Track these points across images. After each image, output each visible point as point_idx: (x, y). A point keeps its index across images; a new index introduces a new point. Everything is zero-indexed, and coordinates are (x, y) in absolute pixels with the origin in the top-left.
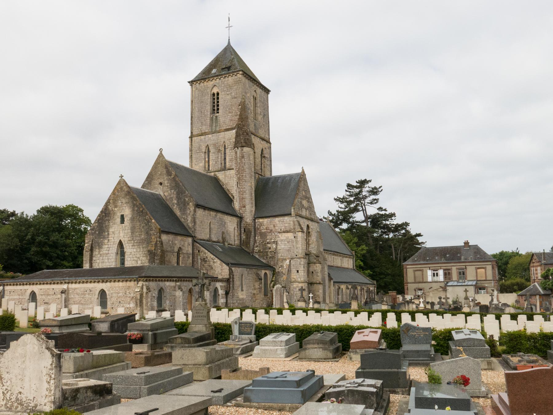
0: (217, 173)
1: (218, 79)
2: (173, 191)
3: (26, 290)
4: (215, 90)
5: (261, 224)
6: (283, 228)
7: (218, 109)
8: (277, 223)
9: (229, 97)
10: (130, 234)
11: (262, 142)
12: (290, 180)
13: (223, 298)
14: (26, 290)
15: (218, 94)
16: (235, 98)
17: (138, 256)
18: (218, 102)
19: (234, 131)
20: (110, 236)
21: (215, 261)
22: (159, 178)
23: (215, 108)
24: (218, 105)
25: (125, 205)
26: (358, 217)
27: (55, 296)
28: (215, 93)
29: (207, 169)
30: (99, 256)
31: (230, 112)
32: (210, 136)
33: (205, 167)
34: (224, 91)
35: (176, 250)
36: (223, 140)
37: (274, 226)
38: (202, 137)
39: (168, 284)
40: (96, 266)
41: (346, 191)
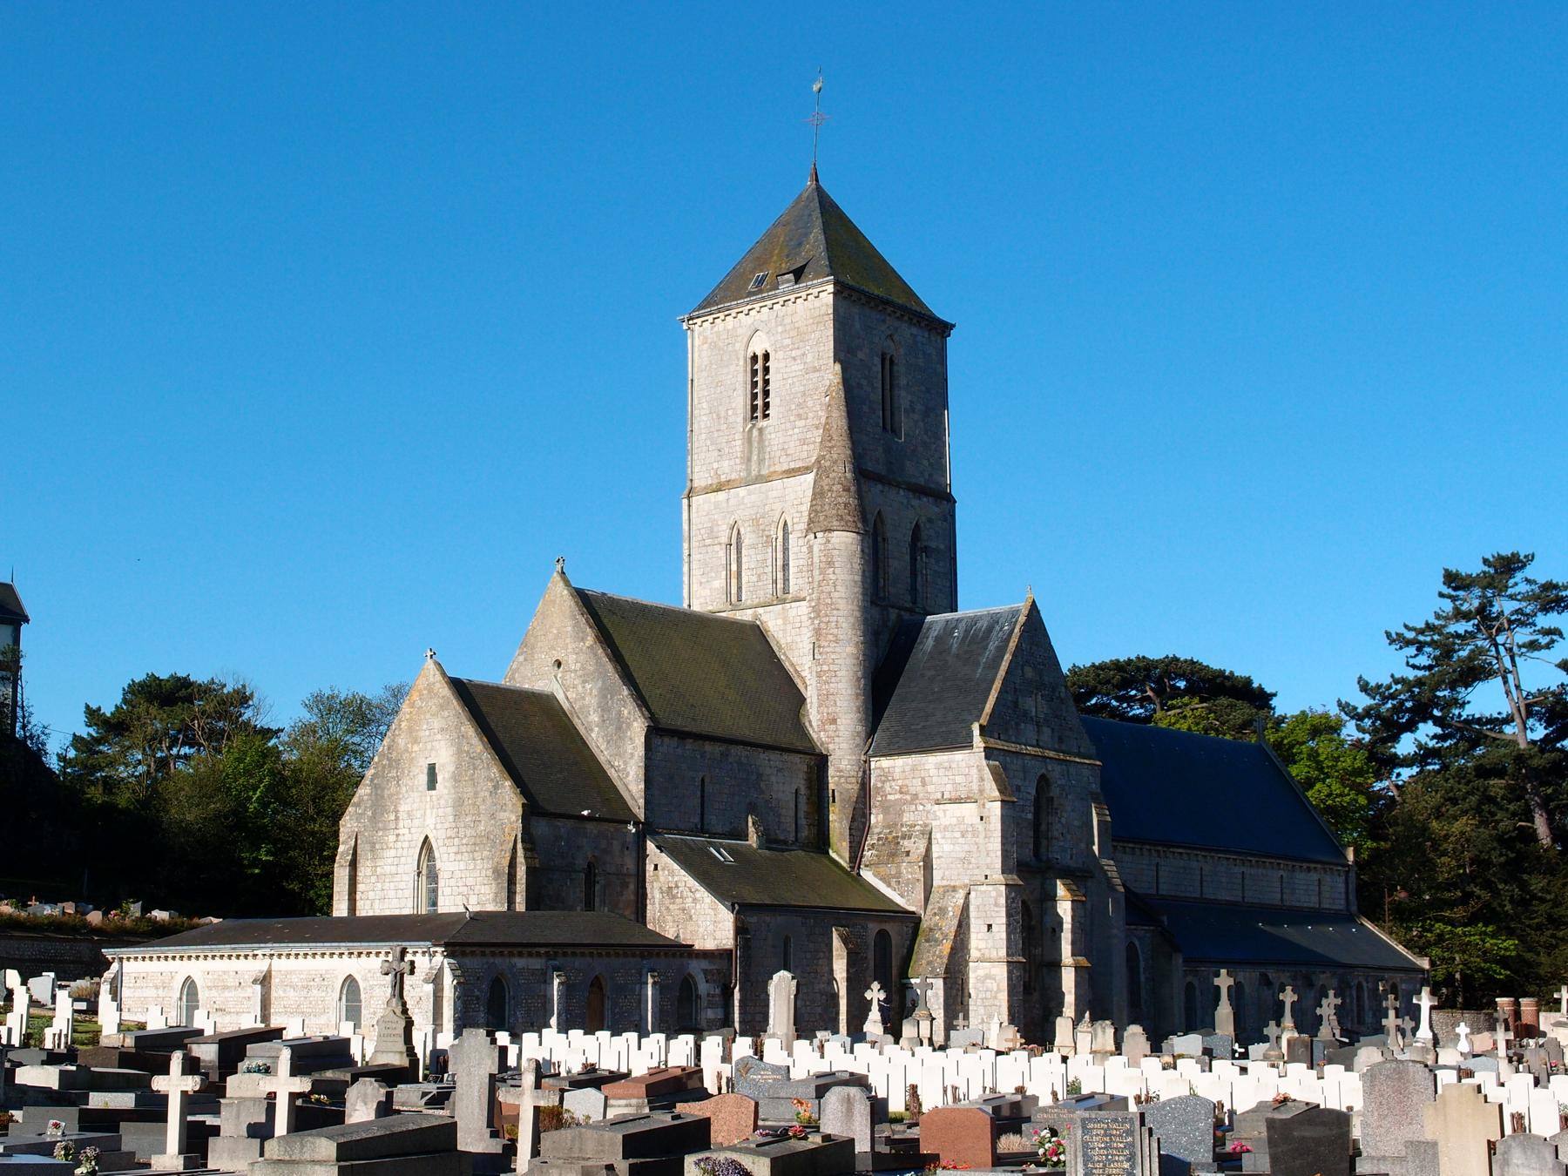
0: (760, 610)
1: (765, 310)
2: (588, 686)
3: (172, 975)
4: (758, 348)
5: (887, 776)
6: (949, 787)
7: (767, 406)
8: (932, 772)
9: (797, 367)
10: (451, 818)
11: (915, 502)
12: (990, 629)
13: (711, 1005)
14: (172, 975)
15: (766, 357)
16: (816, 370)
17: (470, 881)
18: (766, 382)
19: (810, 477)
21: (698, 895)
22: (553, 648)
23: (759, 406)
24: (766, 393)
25: (439, 737)
26: (1485, 700)
27: (241, 993)
28: (760, 354)
29: (734, 599)
30: (373, 879)
31: (799, 416)
32: (742, 491)
33: (728, 593)
34: (783, 347)
35: (581, 863)
36: (778, 507)
37: (924, 784)
38: (721, 496)
39: (520, 963)
40: (364, 910)
41: (1441, 595)
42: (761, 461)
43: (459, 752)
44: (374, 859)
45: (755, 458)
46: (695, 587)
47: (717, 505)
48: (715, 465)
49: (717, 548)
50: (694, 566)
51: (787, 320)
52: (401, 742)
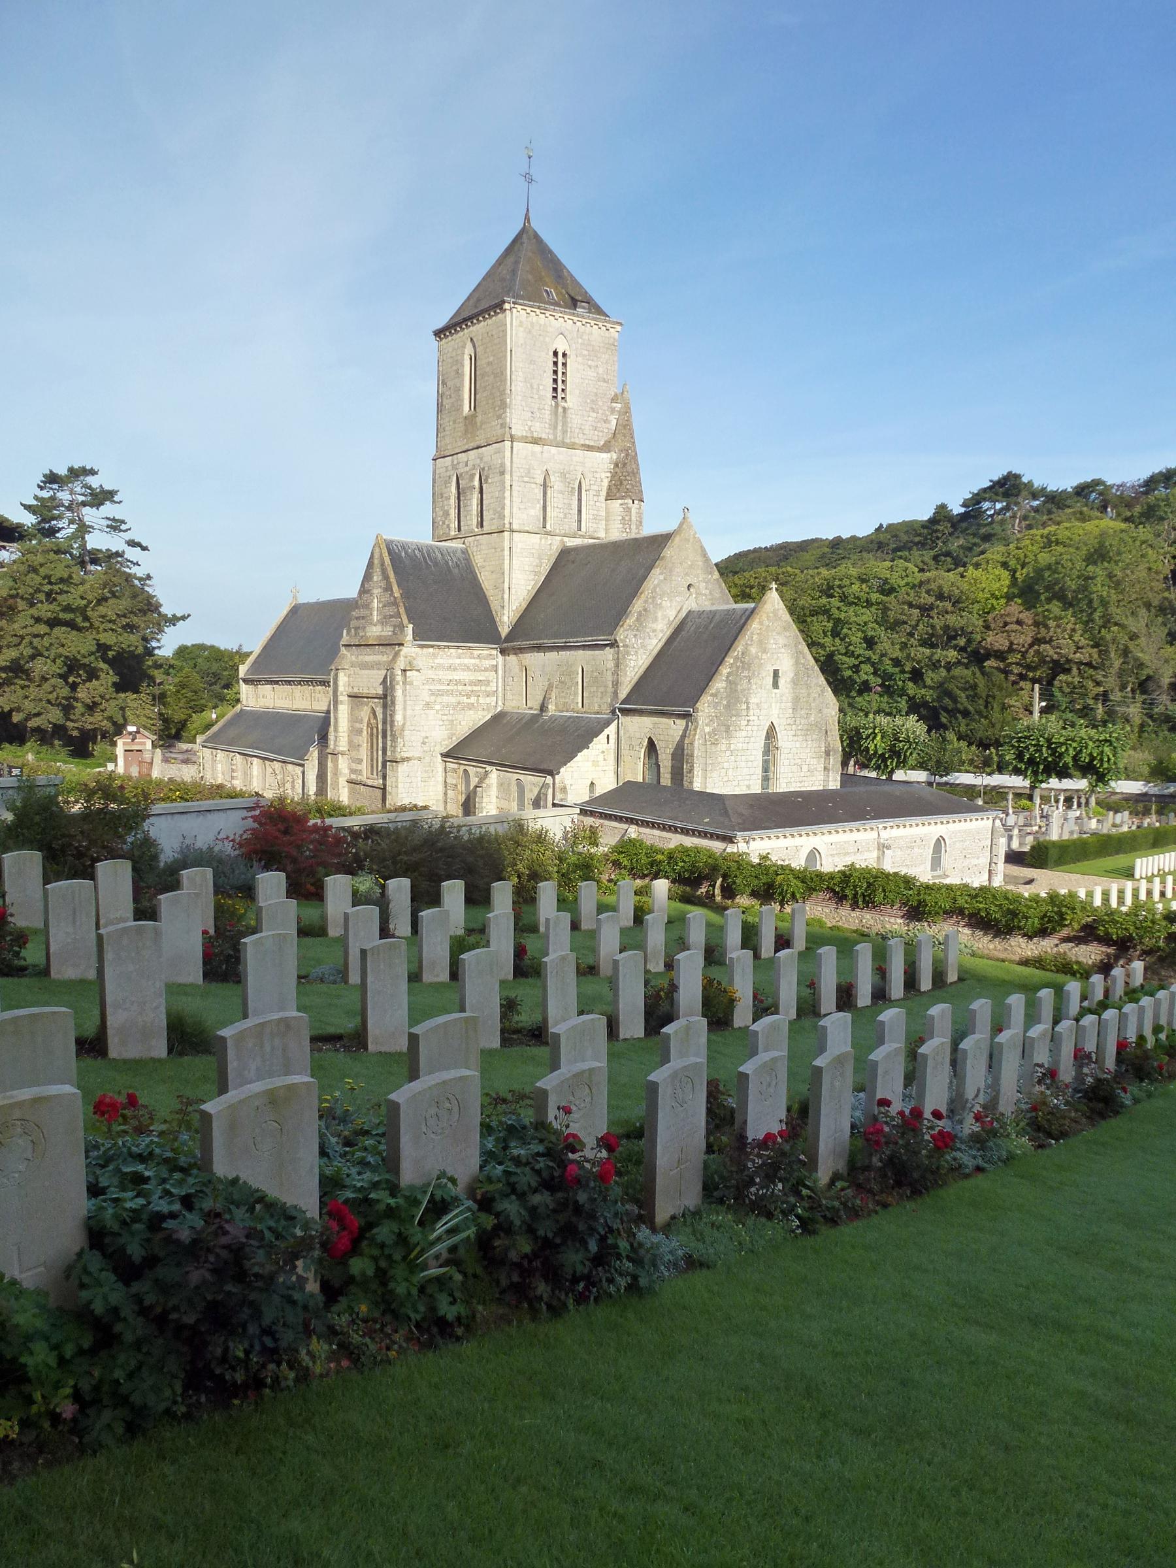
16: (604, 381)
17: (803, 756)
20: (751, 712)
22: (687, 574)
30: (728, 753)
31: (593, 410)
32: (553, 450)
36: (580, 469)
38: (537, 448)
42: (564, 432)
43: (797, 663)
44: (729, 737)
45: (560, 428)
46: (515, 510)
47: (533, 453)
48: (529, 423)
49: (533, 486)
50: (515, 494)
51: (586, 337)
52: (753, 650)
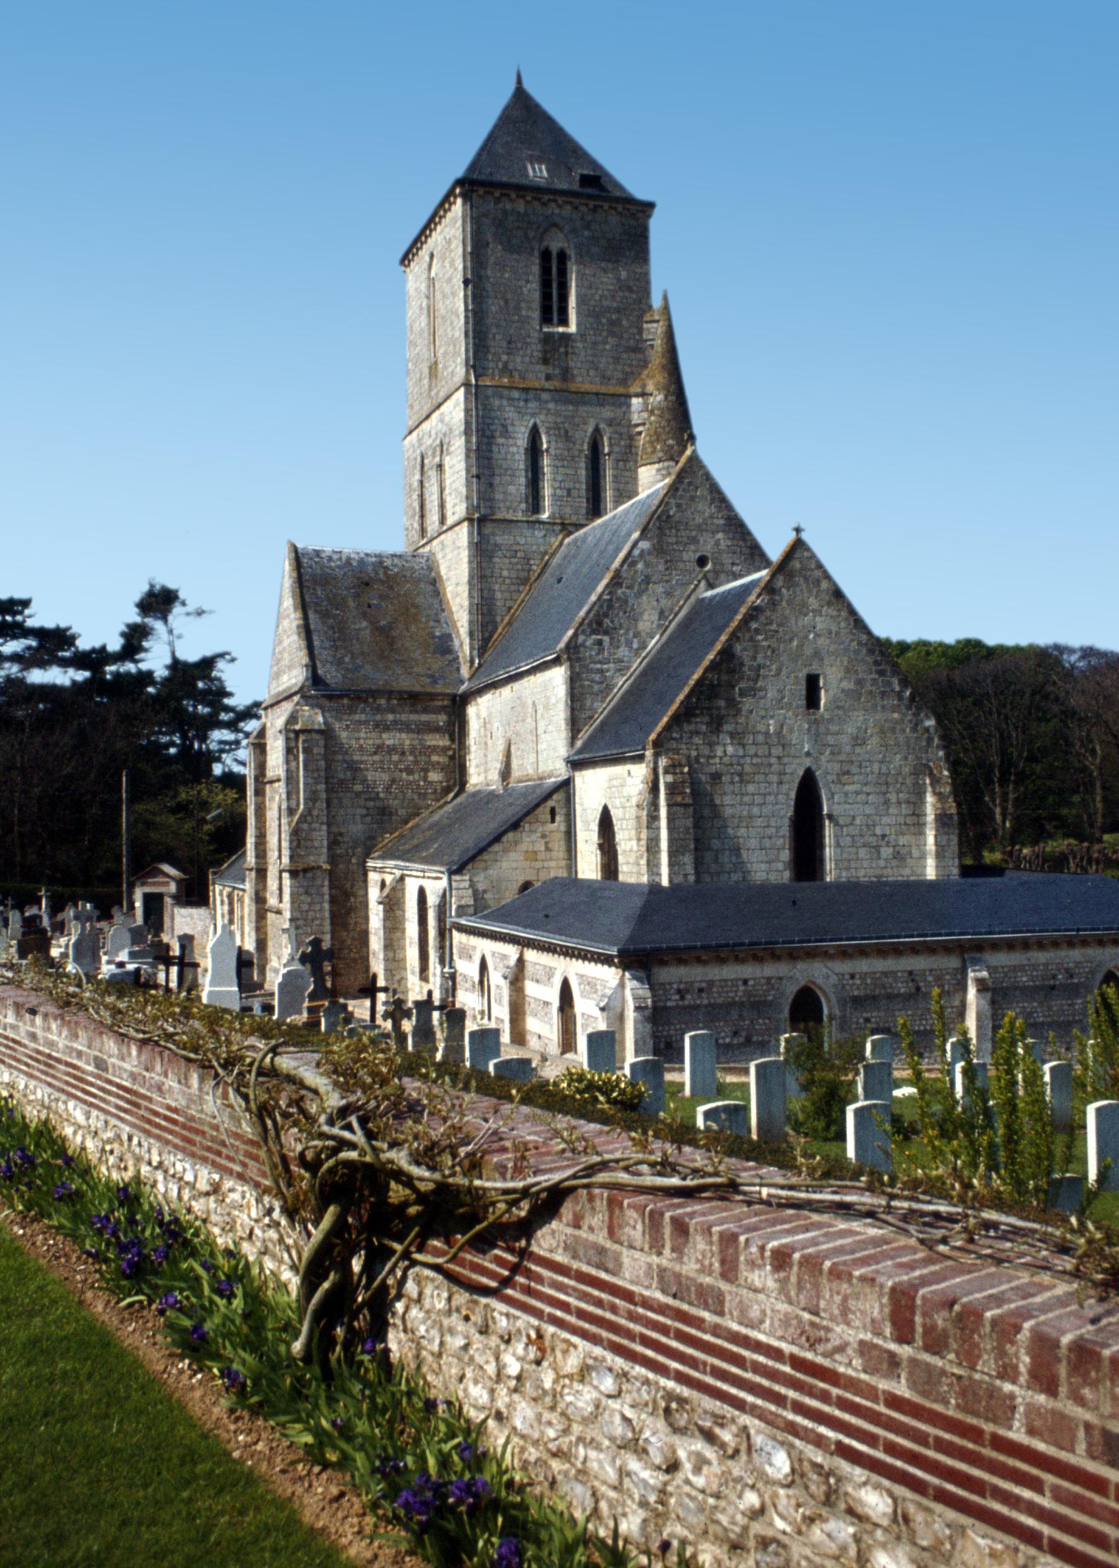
31: (612, 334)
